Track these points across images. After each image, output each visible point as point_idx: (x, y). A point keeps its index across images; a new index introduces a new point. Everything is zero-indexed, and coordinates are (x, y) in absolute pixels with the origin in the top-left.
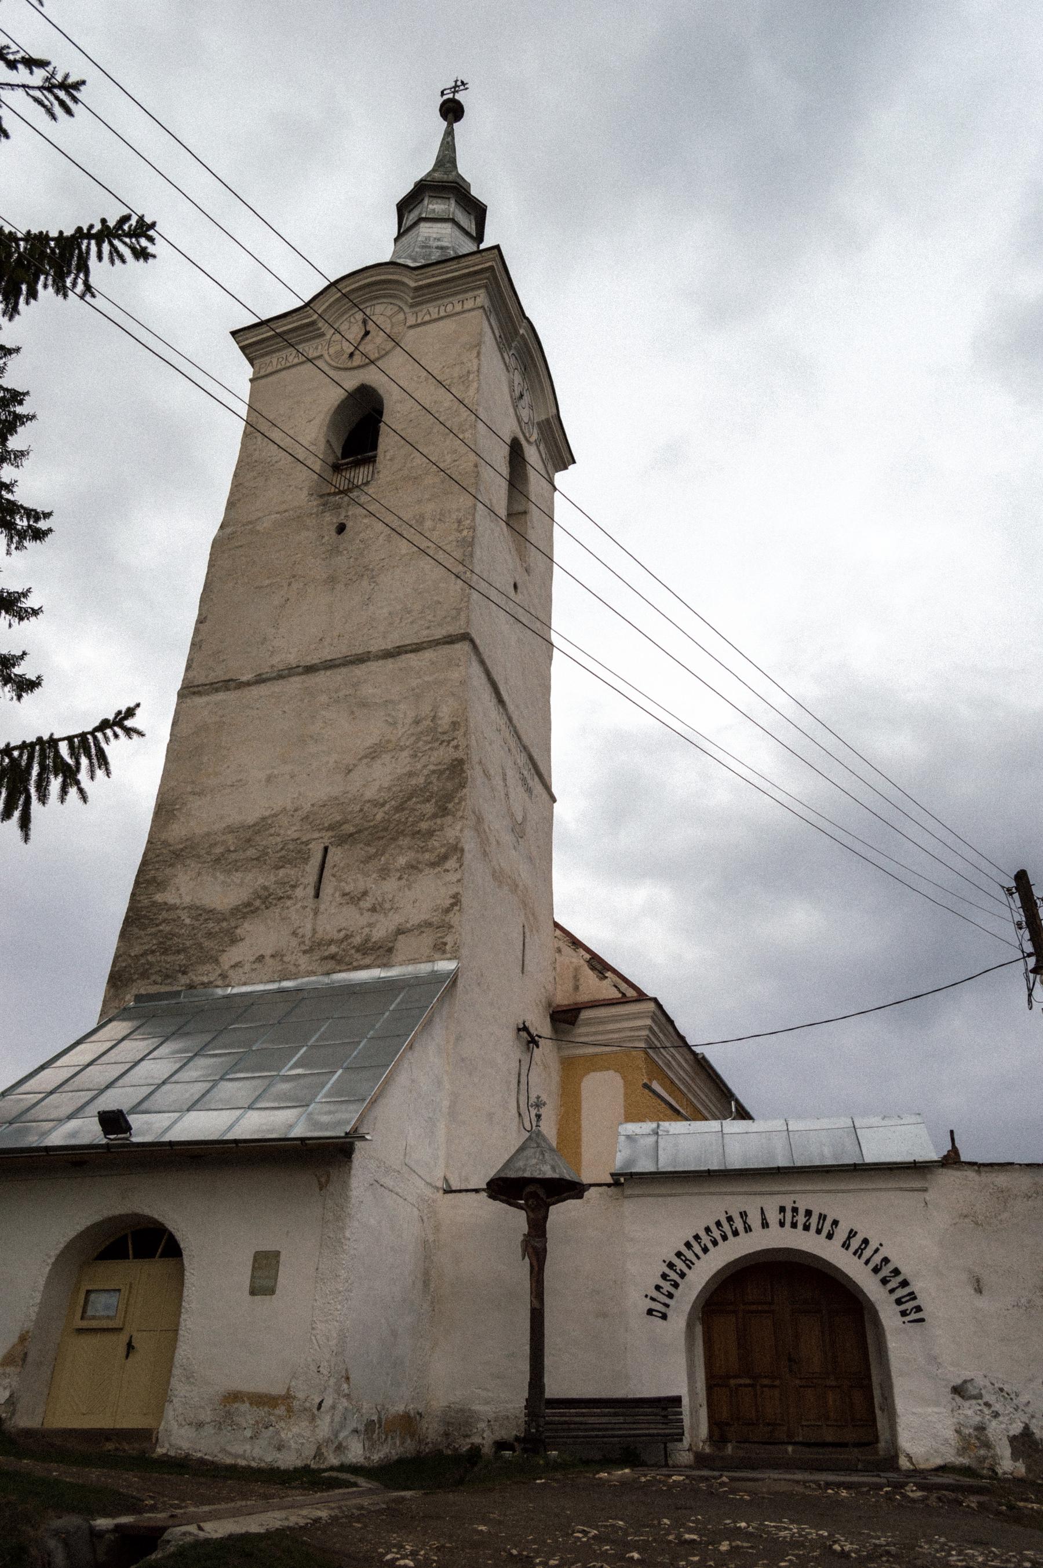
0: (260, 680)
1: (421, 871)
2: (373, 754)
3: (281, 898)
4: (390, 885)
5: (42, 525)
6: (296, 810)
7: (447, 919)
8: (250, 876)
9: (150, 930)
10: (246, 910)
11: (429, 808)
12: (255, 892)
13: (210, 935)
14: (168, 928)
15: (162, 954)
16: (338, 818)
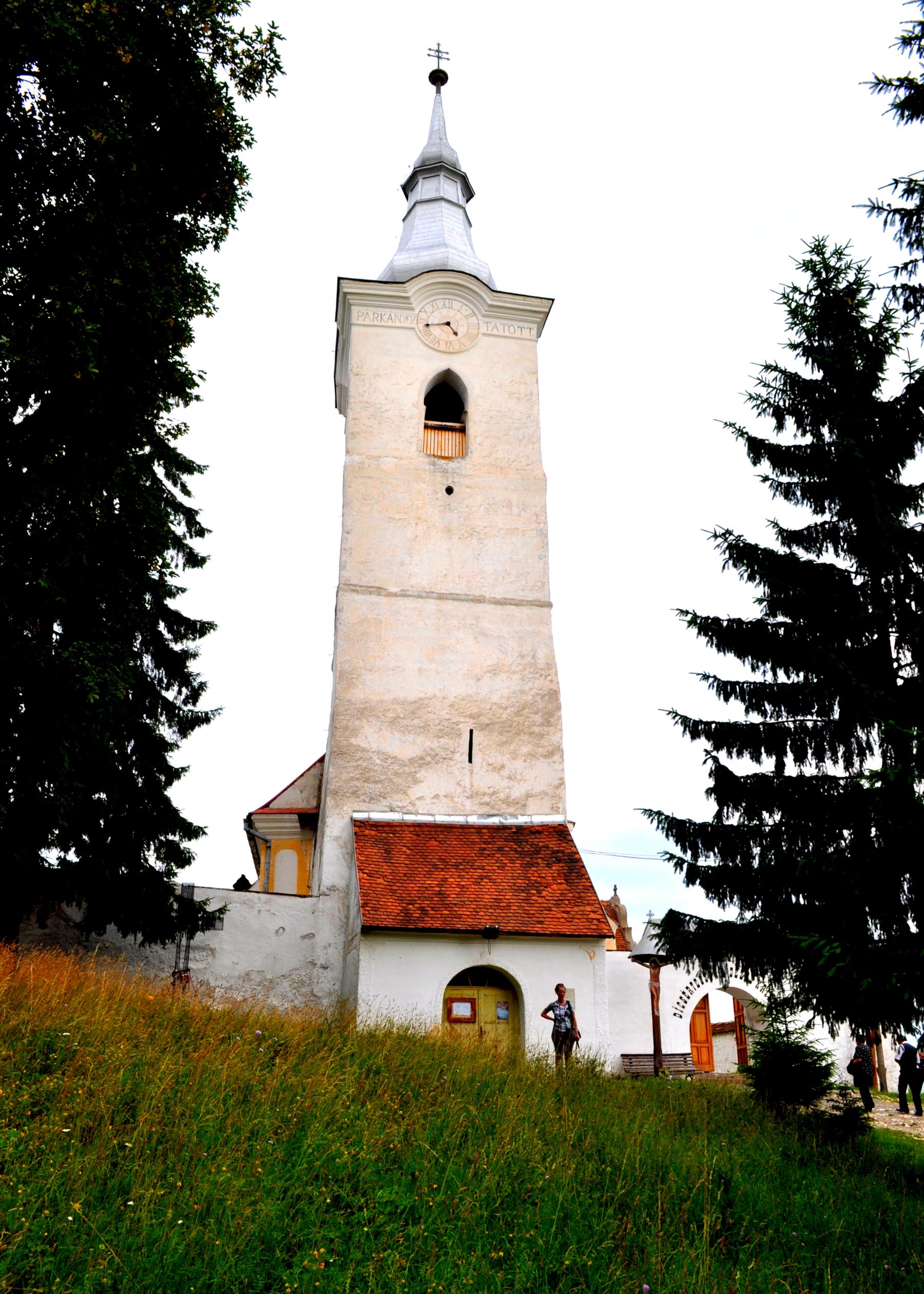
0: (404, 594)
1: (538, 759)
2: (495, 671)
3: (445, 759)
4: (519, 764)
6: (444, 698)
7: (557, 792)
8: (419, 739)
9: (352, 764)
10: (421, 762)
11: (538, 718)
12: (425, 751)
13: (396, 774)
14: (365, 764)
15: (365, 781)
16: (476, 711)
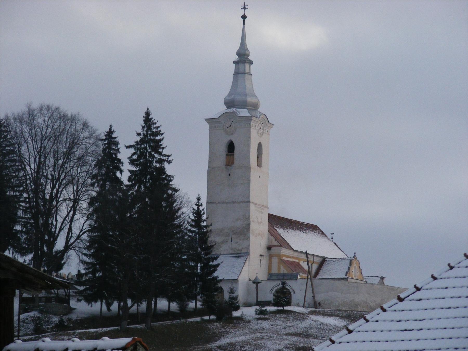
5: (170, 159)
11: (245, 230)
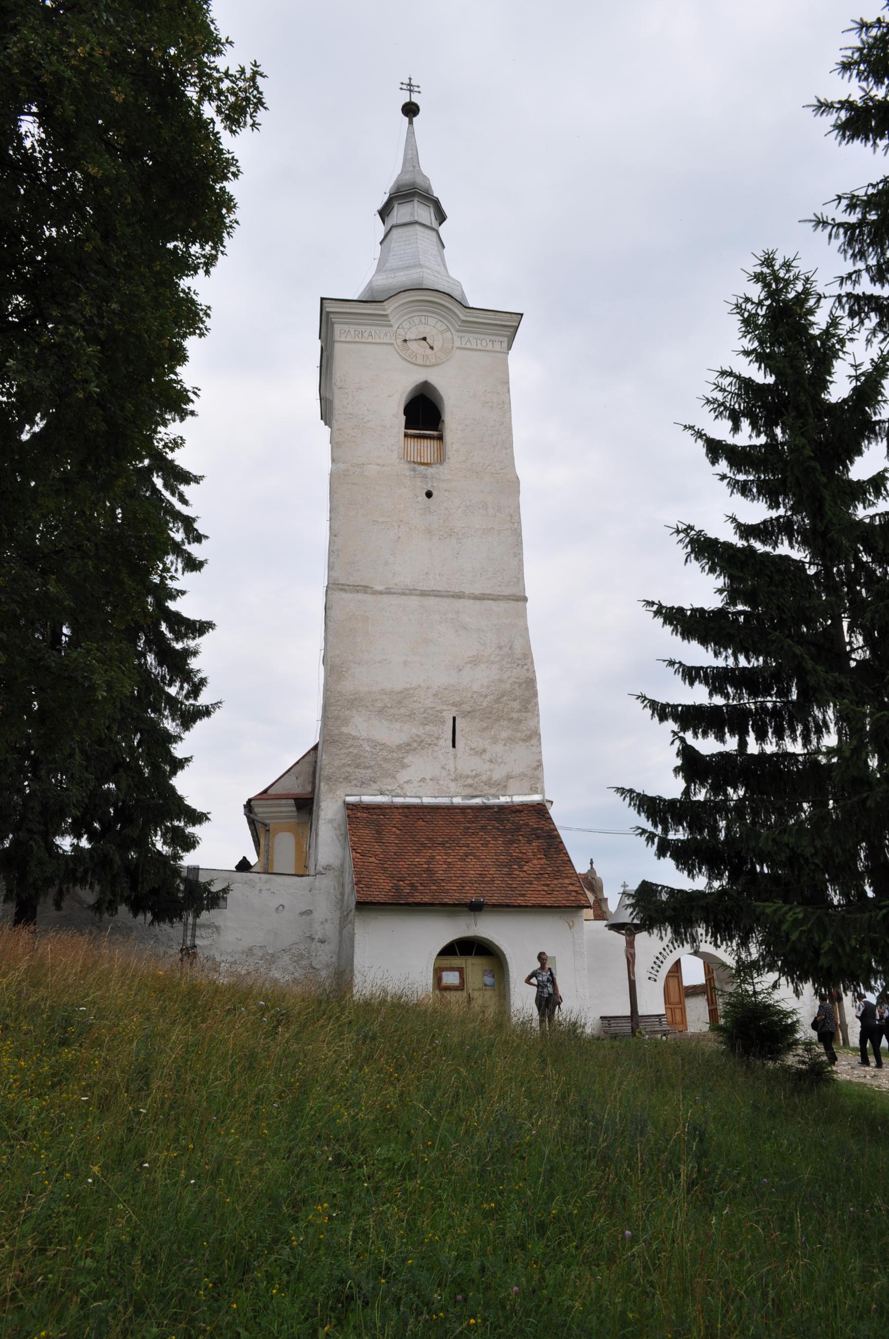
0: (388, 592)
2: (475, 662)
3: (430, 744)
4: (499, 748)
9: (343, 751)
10: (408, 748)
12: (411, 737)
13: (385, 760)
14: (355, 751)
15: (356, 767)
16: (458, 699)
